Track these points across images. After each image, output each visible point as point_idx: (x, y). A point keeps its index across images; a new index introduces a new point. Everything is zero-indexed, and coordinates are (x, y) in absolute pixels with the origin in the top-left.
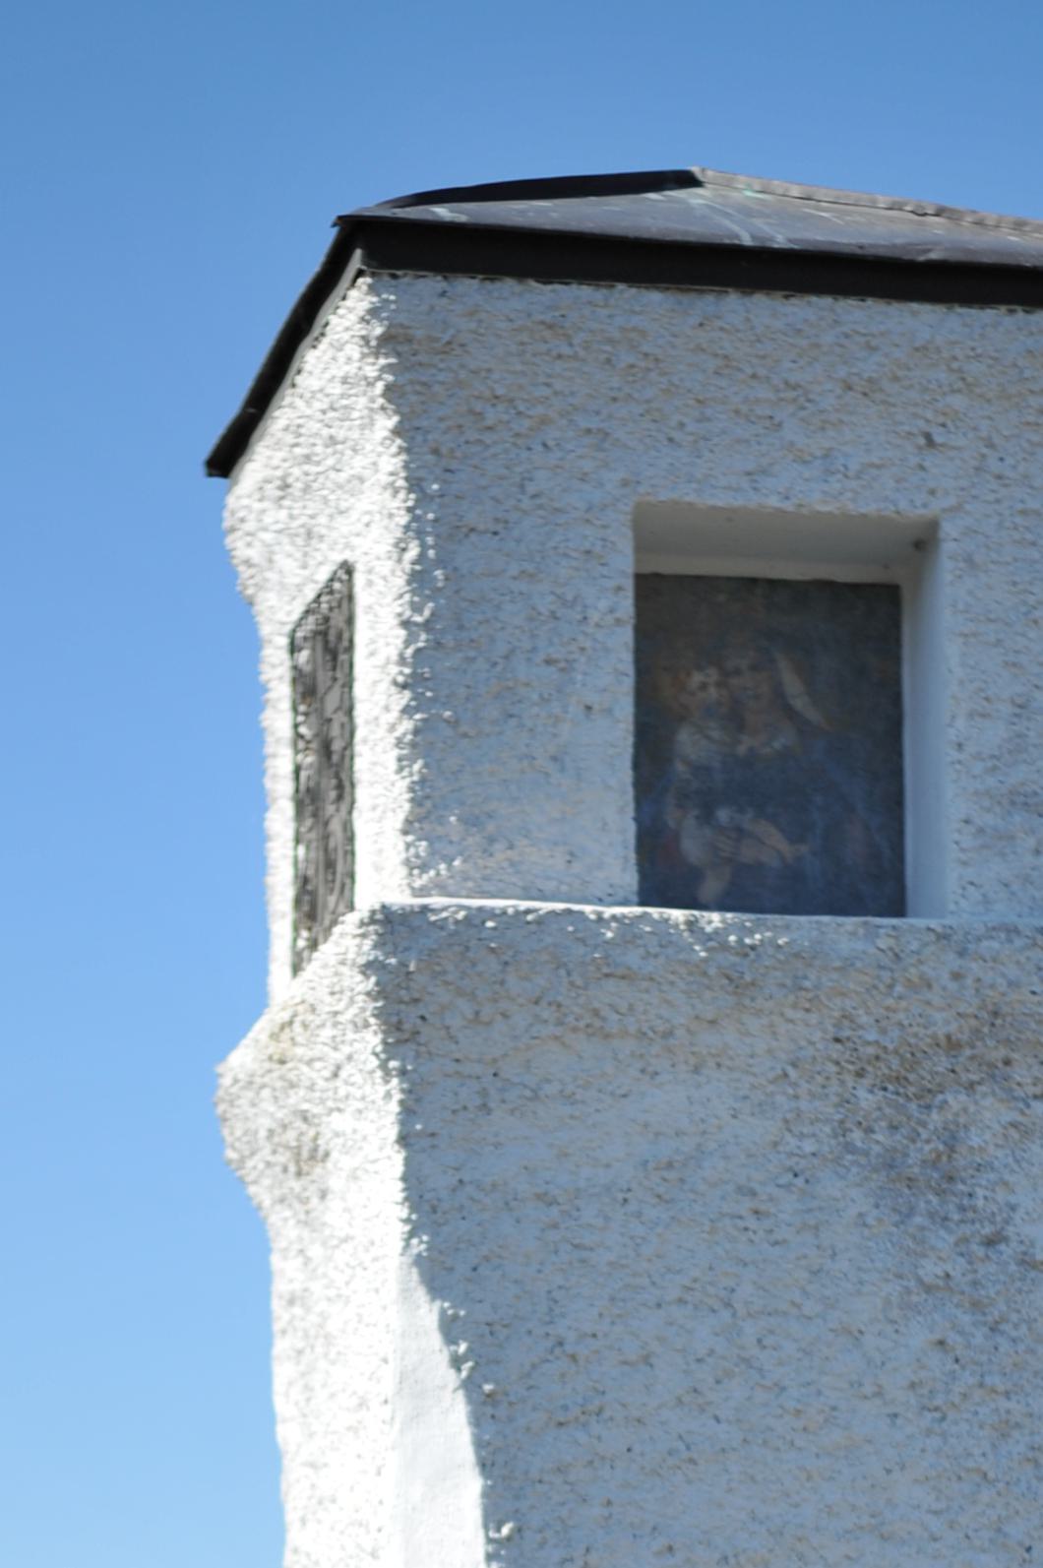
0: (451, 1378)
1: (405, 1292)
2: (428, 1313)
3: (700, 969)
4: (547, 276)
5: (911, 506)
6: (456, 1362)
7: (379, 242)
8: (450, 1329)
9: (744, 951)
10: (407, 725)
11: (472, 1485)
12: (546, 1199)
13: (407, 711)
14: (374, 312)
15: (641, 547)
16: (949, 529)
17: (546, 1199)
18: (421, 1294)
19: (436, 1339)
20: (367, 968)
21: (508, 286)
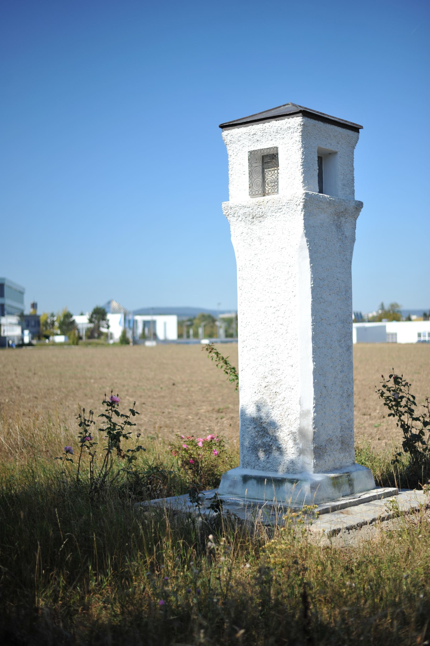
0: (307, 247)
1: (302, 237)
2: (305, 239)
3: (327, 202)
4: (315, 119)
5: (336, 150)
6: (308, 245)
7: (306, 114)
8: (307, 241)
9: (331, 200)
10: (302, 170)
11: (309, 260)
12: (314, 227)
13: (302, 168)
14: (302, 121)
15: (318, 152)
16: (339, 153)
17: (314, 227)
18: (304, 237)
19: (306, 242)
20: (304, 199)
21: (312, 120)
